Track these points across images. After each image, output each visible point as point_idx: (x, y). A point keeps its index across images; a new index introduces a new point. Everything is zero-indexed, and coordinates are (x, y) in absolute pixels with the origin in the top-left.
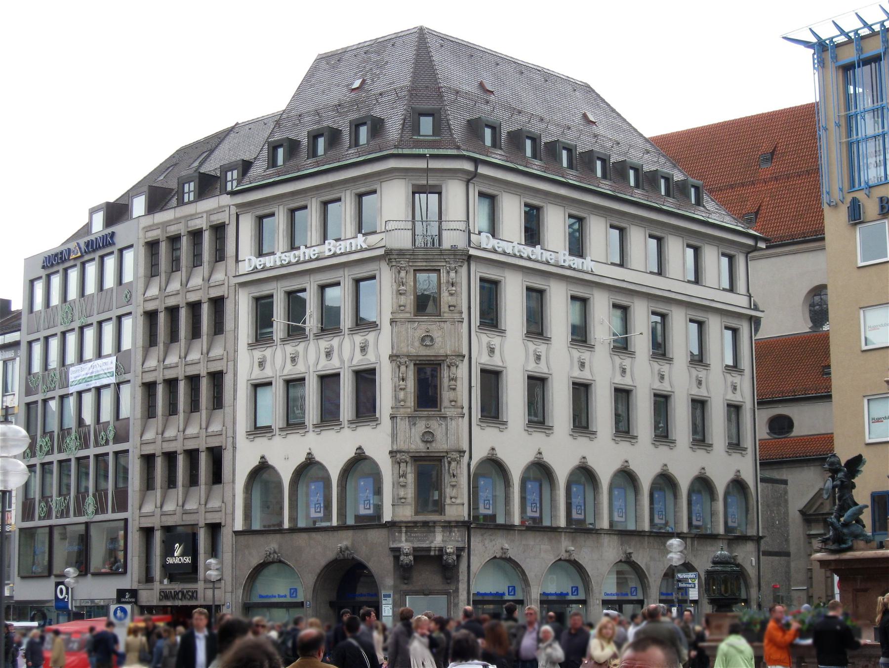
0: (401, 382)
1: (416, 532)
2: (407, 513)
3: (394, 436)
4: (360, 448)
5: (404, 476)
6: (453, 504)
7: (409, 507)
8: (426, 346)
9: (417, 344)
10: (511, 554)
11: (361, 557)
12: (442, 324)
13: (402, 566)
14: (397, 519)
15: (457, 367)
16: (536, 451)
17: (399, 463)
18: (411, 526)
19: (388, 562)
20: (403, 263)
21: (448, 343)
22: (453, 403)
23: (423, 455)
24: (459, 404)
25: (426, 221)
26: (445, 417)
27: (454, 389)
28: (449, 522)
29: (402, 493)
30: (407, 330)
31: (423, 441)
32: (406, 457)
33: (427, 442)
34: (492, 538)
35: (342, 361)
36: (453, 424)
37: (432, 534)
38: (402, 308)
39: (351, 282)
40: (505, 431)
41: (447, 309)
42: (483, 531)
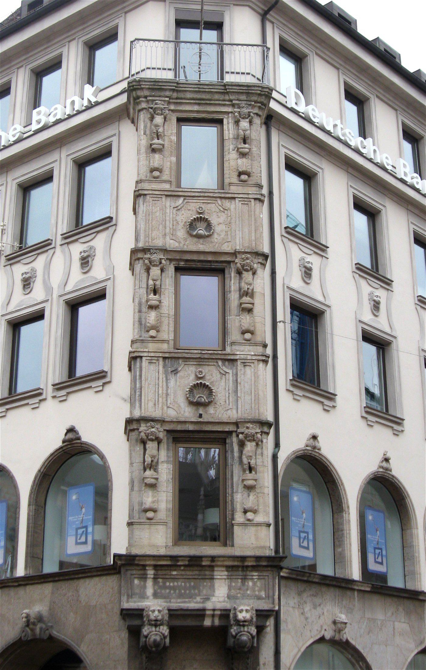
0: (152, 296)
1: (174, 579)
2: (158, 540)
3: (135, 396)
4: (71, 430)
5: (153, 466)
6: (249, 523)
7: (161, 528)
8: (199, 237)
9: (181, 233)
10: (350, 635)
11: (66, 633)
12: (227, 203)
13: (145, 649)
14: (135, 551)
15: (254, 274)
16: (380, 457)
17: (144, 443)
18: (165, 566)
19: (118, 642)
20: (160, 104)
21: (239, 235)
22: (248, 336)
23: (191, 427)
24: (259, 339)
25: (139, 560)
26: (234, 361)
27: (250, 311)
28: (243, 558)
29: (149, 499)
30: (163, 209)
31: (191, 403)
32: (159, 431)
33: (197, 404)
34: (318, 600)
35: (48, 289)
36: (246, 375)
37: (207, 583)
38: (156, 173)
39: (70, 164)
40: (332, 411)
41: (235, 180)
42: (301, 586)
